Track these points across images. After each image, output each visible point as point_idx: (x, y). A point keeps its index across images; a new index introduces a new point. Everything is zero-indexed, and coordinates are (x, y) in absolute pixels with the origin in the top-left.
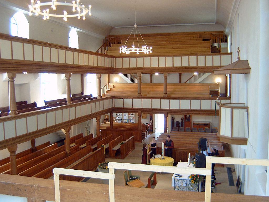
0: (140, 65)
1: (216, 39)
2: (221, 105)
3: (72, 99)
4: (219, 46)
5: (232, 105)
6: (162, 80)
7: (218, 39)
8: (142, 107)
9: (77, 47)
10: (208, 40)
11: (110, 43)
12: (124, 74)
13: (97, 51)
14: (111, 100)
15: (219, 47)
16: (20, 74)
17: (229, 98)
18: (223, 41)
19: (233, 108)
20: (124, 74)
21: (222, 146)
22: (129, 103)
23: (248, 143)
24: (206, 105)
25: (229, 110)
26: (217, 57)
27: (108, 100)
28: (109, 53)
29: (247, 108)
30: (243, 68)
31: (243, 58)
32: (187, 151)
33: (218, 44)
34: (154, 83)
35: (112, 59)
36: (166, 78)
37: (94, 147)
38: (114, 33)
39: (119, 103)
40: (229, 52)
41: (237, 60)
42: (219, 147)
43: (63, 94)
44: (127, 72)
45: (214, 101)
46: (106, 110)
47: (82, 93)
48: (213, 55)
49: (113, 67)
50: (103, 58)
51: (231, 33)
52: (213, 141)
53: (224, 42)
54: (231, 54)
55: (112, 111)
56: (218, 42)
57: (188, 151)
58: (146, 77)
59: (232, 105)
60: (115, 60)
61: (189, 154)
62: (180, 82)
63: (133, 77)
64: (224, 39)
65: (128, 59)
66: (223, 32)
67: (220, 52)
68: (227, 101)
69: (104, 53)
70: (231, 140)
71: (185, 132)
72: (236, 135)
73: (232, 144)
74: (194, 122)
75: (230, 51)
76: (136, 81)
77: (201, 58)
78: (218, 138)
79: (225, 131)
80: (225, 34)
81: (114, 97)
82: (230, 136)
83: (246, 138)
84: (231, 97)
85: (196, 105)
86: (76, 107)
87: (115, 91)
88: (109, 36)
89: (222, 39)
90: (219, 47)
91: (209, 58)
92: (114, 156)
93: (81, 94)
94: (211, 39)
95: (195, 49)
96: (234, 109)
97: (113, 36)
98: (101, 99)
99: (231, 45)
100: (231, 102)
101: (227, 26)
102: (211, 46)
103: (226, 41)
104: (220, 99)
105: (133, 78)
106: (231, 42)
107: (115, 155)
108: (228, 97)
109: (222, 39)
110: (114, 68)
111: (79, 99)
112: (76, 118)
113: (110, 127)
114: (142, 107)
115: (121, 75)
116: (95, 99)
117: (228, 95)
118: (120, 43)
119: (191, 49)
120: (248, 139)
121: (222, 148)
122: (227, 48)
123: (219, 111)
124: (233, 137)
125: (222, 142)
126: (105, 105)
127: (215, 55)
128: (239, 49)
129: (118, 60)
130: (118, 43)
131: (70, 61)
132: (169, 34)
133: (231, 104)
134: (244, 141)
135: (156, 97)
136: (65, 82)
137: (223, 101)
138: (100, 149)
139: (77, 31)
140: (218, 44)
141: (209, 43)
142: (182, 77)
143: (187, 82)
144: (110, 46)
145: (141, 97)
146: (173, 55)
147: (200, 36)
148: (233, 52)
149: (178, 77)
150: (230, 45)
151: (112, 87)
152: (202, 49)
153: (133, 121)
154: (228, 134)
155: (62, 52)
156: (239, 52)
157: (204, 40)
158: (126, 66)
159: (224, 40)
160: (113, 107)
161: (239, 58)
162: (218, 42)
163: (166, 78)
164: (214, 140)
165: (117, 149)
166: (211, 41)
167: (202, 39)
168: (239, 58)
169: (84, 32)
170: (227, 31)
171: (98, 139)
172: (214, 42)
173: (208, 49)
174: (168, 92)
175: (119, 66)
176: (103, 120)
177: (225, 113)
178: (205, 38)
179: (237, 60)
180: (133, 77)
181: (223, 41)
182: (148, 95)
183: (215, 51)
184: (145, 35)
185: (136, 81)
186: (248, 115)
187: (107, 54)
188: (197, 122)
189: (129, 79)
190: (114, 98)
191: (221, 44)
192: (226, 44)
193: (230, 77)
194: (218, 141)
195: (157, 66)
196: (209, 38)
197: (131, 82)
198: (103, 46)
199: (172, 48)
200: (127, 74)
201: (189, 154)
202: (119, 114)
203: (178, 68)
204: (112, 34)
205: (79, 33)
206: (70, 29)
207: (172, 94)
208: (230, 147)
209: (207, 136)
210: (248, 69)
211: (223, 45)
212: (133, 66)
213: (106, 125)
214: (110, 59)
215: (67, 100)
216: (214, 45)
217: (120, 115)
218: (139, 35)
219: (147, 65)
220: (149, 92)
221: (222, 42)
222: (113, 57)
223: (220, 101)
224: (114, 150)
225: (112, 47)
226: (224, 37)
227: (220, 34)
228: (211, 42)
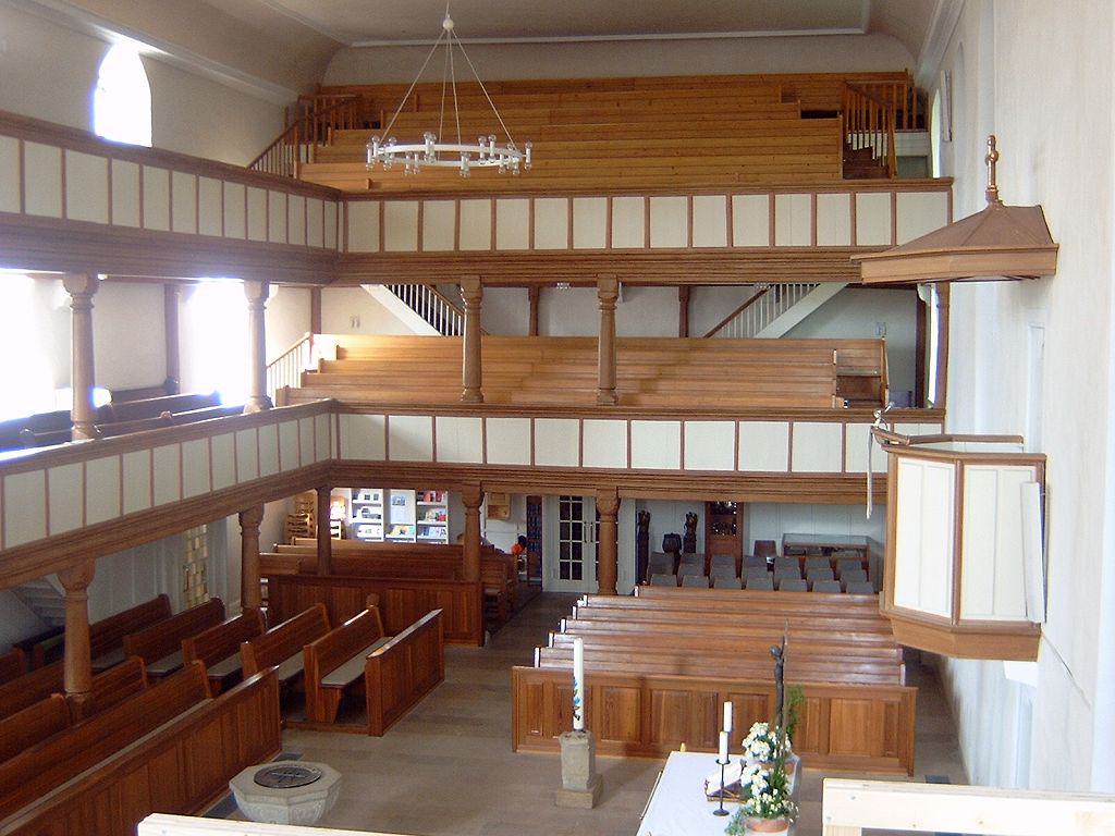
0: (476, 240)
1: (867, 112)
2: (901, 445)
3: (103, 420)
4: (885, 146)
5: (957, 446)
6: (592, 326)
7: (880, 112)
8: (485, 461)
9: (139, 133)
10: (833, 114)
11: (320, 125)
12: (396, 287)
13: (257, 161)
14: (322, 419)
15: (885, 151)
16: (181, 372)
17: (938, 415)
18: (905, 123)
19: (961, 461)
20: (396, 287)
21: (903, 668)
22: (415, 435)
23: (1044, 648)
24: (819, 448)
25: (940, 475)
26: (874, 203)
27: (306, 422)
28: (314, 173)
29: (1039, 462)
30: (1020, 246)
31: (1016, 195)
32: (715, 690)
33: (873, 139)
34: (553, 333)
35: (330, 206)
36: (609, 310)
37: (220, 670)
38: (340, 75)
39: (360, 441)
40: (936, 174)
41: (982, 205)
42: (886, 669)
43: (61, 385)
44: (417, 276)
45: (859, 432)
46: (296, 472)
47: (170, 385)
48: (853, 191)
49: (330, 245)
50: (277, 197)
51: (950, 79)
52: (854, 637)
53: (910, 126)
54: (946, 184)
55: (330, 478)
56: (880, 128)
57: (723, 691)
58: (513, 306)
59: (957, 446)
60: (346, 208)
61: (728, 707)
62: (685, 331)
63: (439, 303)
64: (910, 110)
65: (413, 205)
66: (904, 75)
67: (889, 177)
68: (931, 429)
69: (292, 176)
70: (952, 637)
71: (711, 593)
72: (976, 610)
73: (960, 655)
74: (788, 540)
75: (942, 169)
76: (438, 309)
77: (794, 206)
78: (882, 623)
79: (918, 588)
80: (916, 85)
81: (336, 407)
82: (949, 615)
83: (1032, 624)
84: (948, 408)
85: (764, 448)
86: (125, 456)
87: (346, 373)
88: (320, 89)
89: (900, 112)
90: (885, 151)
91: (835, 205)
92: (332, 720)
93: (162, 387)
94: (842, 112)
95: (761, 159)
96: (968, 468)
97: (340, 89)
98: (267, 415)
99: (948, 138)
100: (948, 432)
101: (927, 45)
102: (847, 147)
103: (922, 124)
104: (890, 417)
105: (445, 311)
106: (946, 122)
107: (339, 713)
108: (930, 407)
109: (900, 112)
110: (340, 250)
111: (146, 415)
112: (122, 517)
113: (316, 561)
114: (485, 461)
115: (380, 293)
116: (234, 422)
117: (932, 396)
118: (377, 125)
119: (741, 159)
120: (1044, 628)
121: (899, 675)
122: (926, 160)
123: (890, 480)
124: (963, 616)
125: (903, 643)
126: (287, 450)
127: (867, 189)
128: (993, 145)
129: (363, 214)
130: (365, 128)
131: (88, 208)
132: (628, 84)
133: (950, 439)
134: (1019, 641)
135: (555, 409)
136: (68, 324)
137: (907, 429)
138: (255, 679)
139: (147, 60)
140: (873, 139)
141: (836, 130)
142: (694, 306)
143: (721, 334)
144: (322, 138)
145: (479, 405)
146: (648, 190)
147: (787, 97)
148: (956, 174)
149: (677, 305)
150: (942, 140)
151: (331, 356)
152: (797, 158)
153: (438, 534)
154: (936, 605)
155: (42, 155)
156: (994, 163)
157: (806, 115)
158: (402, 242)
159: (910, 117)
160: (334, 457)
161: (993, 195)
162: (880, 128)
163: (609, 310)
164: (859, 630)
165: (343, 683)
166: (844, 119)
167: (799, 112)
168: (993, 195)
169: (167, 58)
170: (924, 71)
171: (249, 626)
172: (858, 124)
173: (830, 159)
174: (620, 384)
175: (362, 240)
176: (283, 524)
177: (921, 489)
178: (812, 107)
179: (987, 204)
180: (439, 303)
181: (905, 123)
182: (518, 399)
183: (862, 170)
184: (504, 89)
185: (438, 309)
186: (1043, 499)
187: (305, 178)
188: (802, 541)
189: (420, 313)
190: (337, 413)
191: (897, 136)
192: (920, 136)
193: (944, 307)
194: (880, 639)
195: (563, 245)
196: (837, 107)
197: (431, 331)
198: (286, 136)
199: (645, 153)
200: (408, 287)
201: (728, 707)
202: (367, 497)
203: (675, 257)
204: (332, 78)
205: (153, 65)
206: (105, 44)
207: (644, 391)
208: (944, 668)
209: (819, 609)
210: (1041, 250)
211: (905, 143)
212: (439, 241)
213: (299, 551)
214: (315, 204)
215: (75, 417)
216: (858, 141)
217: (372, 501)
218: (468, 89)
219: (513, 239)
220: (523, 379)
221: (899, 126)
222: (337, 196)
223: (893, 427)
224: (333, 688)
225: (332, 144)
226: (910, 101)
227: (890, 86)
228: (844, 129)
